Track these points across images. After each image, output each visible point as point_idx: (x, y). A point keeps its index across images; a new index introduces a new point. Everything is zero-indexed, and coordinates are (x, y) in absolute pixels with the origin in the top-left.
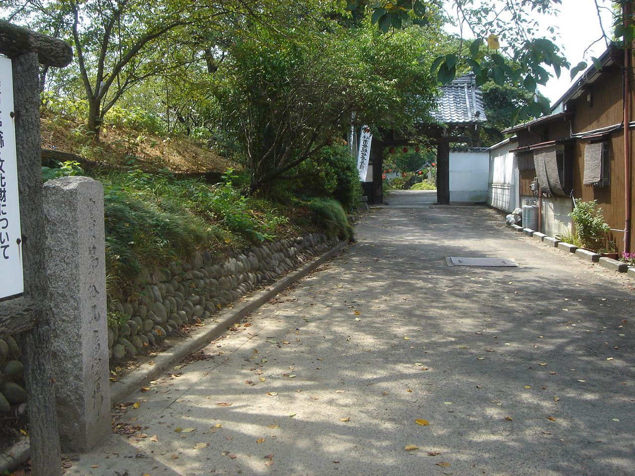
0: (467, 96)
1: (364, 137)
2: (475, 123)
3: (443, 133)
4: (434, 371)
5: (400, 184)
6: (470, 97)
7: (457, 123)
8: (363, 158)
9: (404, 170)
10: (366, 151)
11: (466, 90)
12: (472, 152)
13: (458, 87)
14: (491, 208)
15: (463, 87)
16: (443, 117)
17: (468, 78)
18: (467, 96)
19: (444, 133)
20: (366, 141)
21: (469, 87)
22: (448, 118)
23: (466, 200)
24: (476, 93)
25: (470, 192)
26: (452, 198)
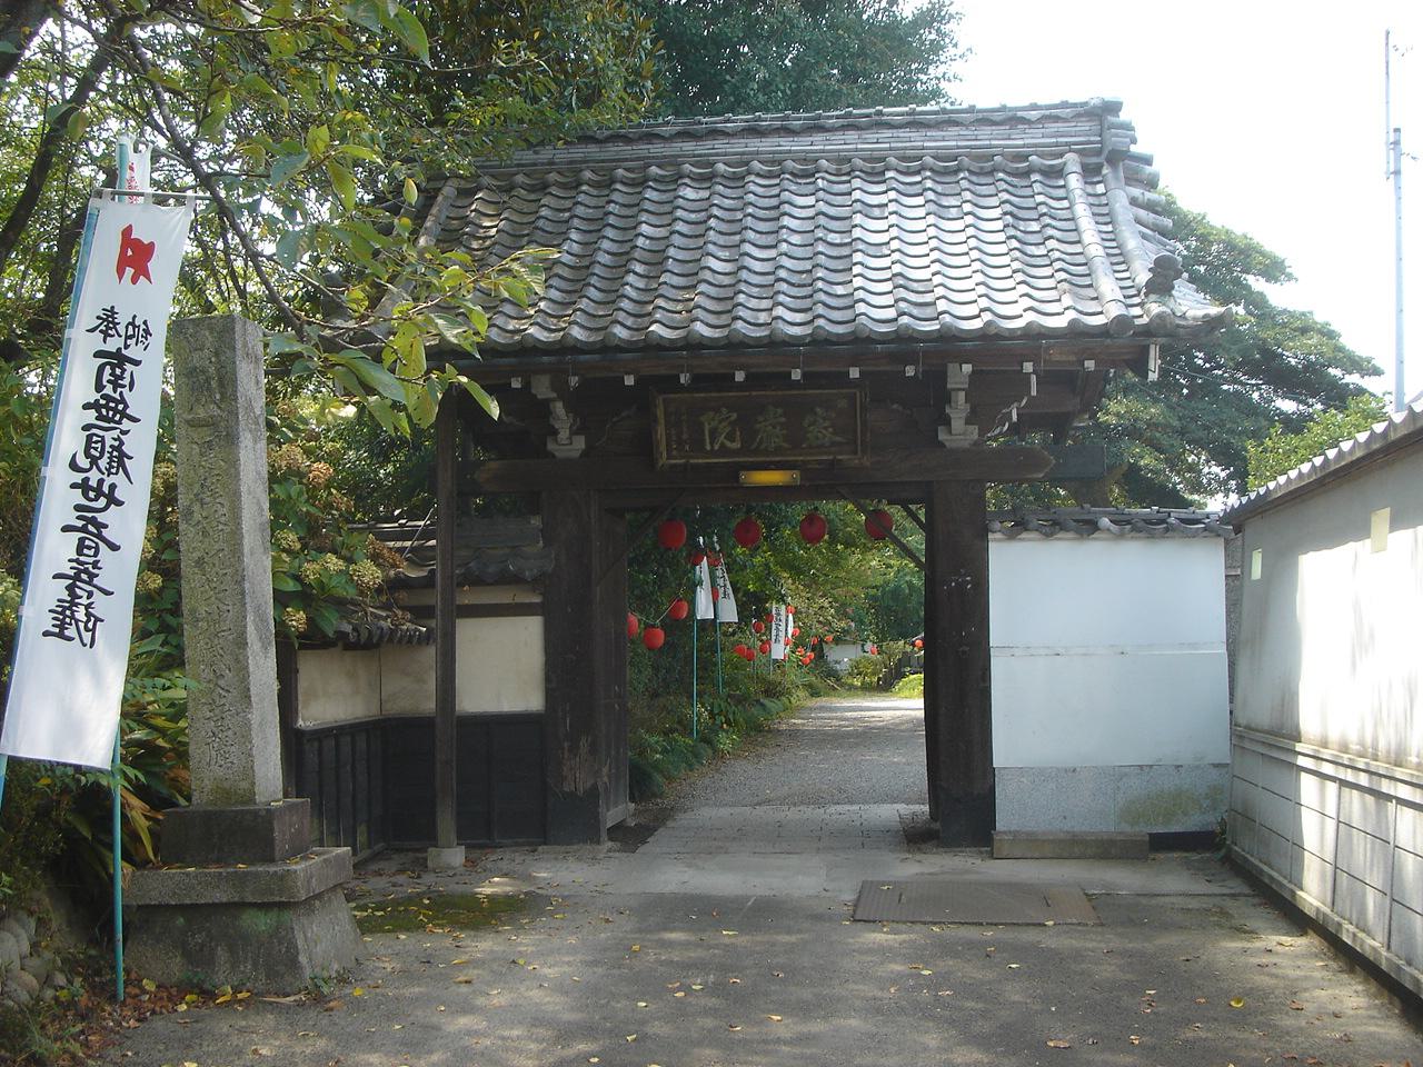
0: (1082, 210)
1: (108, 321)
2: (1148, 332)
3: (947, 422)
4: (1021, 999)
5: (874, 674)
6: (1105, 215)
7: (1033, 335)
8: (89, 530)
9: (881, 638)
10: (120, 458)
11: (1074, 181)
12: (1121, 536)
13: (1026, 174)
14: (1299, 920)
15: (1059, 172)
16: (942, 305)
17: (1084, 126)
18: (1082, 210)
19: (958, 424)
20: (119, 359)
21: (1090, 173)
22: (972, 310)
23: (1106, 824)
24: (1134, 202)
25: (1118, 774)
26: (1006, 818)
